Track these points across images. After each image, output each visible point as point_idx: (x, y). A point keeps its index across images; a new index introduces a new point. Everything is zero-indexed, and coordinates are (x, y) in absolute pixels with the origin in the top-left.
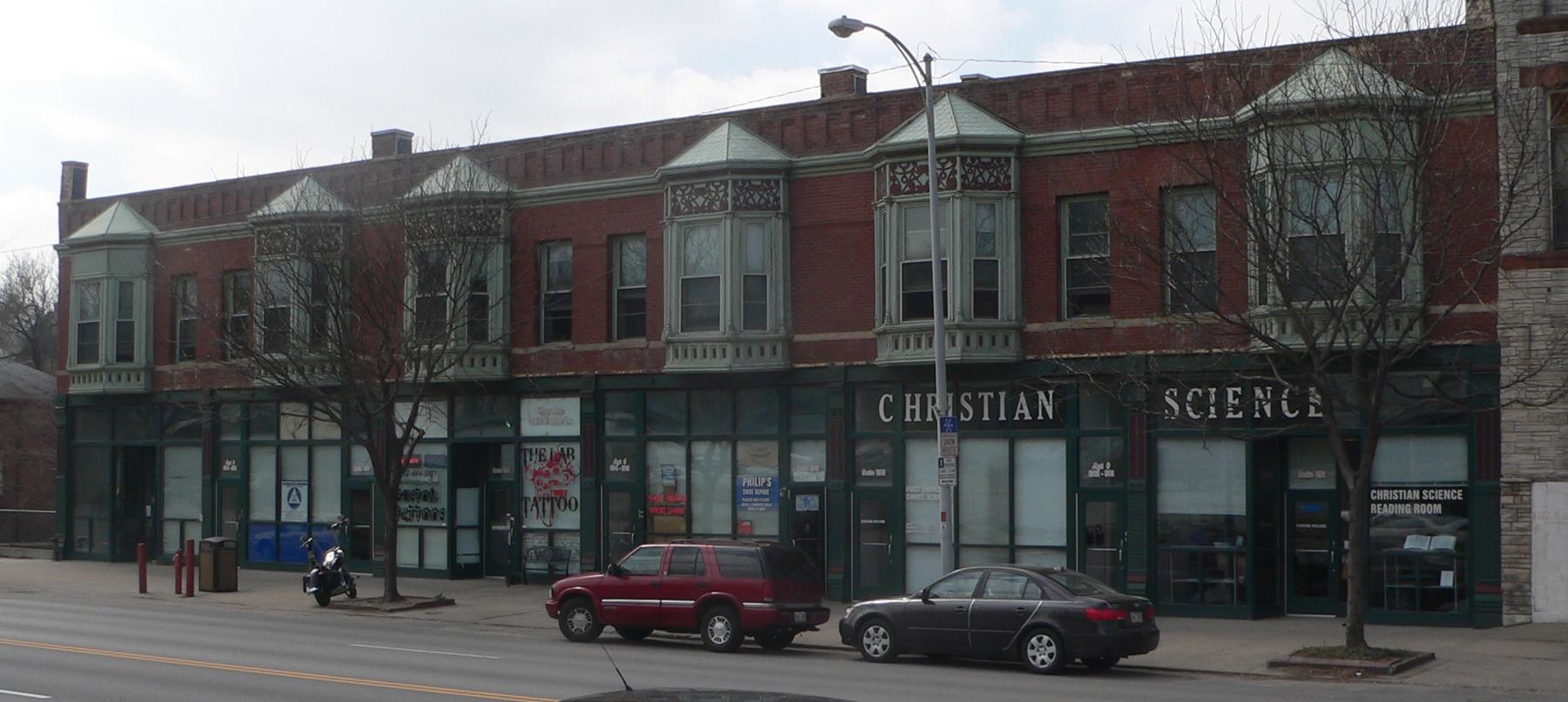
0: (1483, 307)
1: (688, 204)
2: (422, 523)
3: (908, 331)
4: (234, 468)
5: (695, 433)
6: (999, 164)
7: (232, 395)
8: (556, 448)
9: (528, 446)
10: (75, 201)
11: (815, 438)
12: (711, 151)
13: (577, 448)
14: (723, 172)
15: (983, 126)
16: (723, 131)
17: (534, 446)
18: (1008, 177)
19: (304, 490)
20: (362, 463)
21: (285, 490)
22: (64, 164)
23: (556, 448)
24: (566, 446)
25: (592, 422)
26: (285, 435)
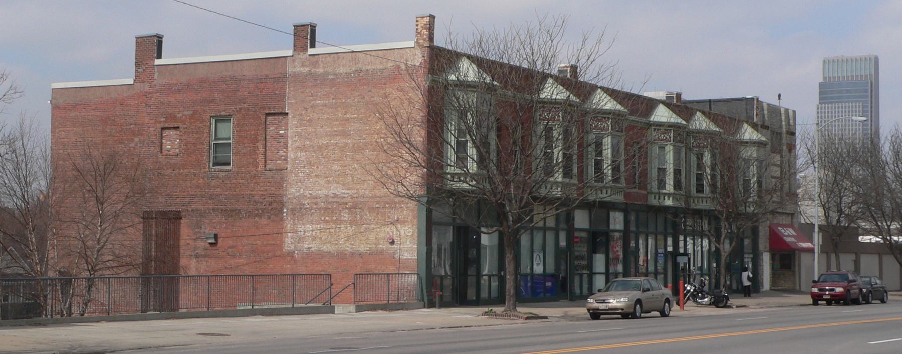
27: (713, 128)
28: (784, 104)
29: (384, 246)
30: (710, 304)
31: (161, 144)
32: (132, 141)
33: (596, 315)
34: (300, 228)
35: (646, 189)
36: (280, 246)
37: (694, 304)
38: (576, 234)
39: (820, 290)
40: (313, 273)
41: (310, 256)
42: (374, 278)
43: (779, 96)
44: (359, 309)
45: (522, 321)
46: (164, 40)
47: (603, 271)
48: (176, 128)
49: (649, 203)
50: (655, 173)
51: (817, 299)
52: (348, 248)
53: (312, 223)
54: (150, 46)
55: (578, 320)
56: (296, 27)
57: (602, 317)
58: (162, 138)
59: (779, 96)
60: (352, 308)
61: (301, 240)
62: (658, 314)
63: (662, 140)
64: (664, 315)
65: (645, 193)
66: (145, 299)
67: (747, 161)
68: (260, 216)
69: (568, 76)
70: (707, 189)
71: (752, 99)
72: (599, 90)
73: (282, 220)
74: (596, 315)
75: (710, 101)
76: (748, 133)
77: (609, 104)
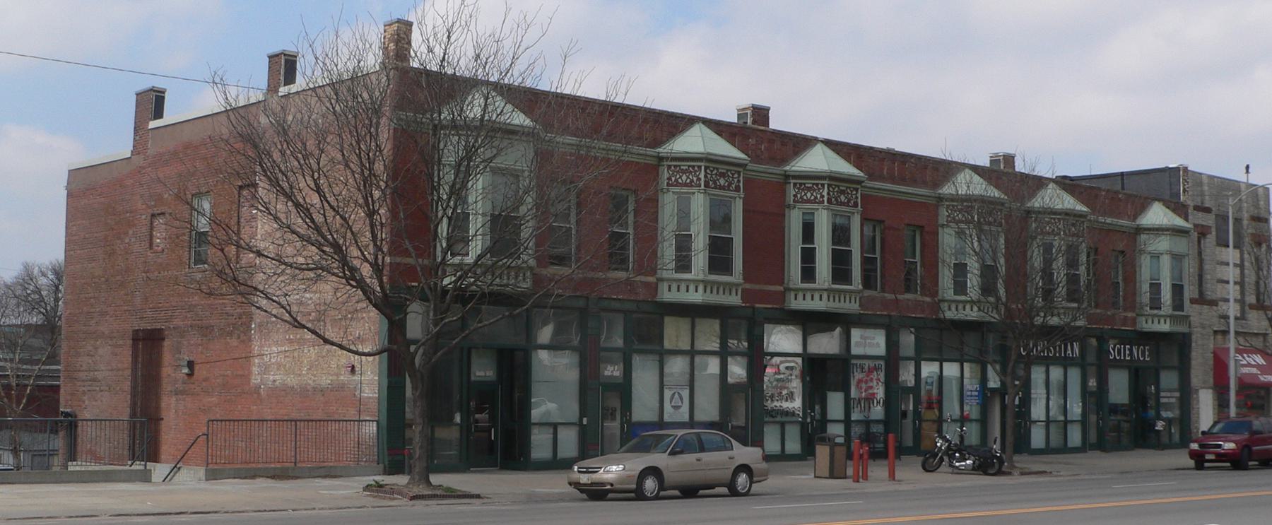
0: (398, 260)
1: (715, 183)
2: (785, 419)
3: (709, 282)
4: (617, 374)
5: (924, 356)
6: (969, 210)
7: (617, 305)
8: (872, 363)
9: (854, 361)
10: (284, 66)
11: (573, 349)
12: (692, 142)
13: (882, 363)
14: (823, 178)
15: (844, 167)
16: (697, 129)
17: (859, 362)
18: (699, 179)
19: (686, 394)
20: (737, 371)
21: (668, 394)
22: (768, 109)
23: (872, 363)
24: (877, 362)
25: (892, 344)
26: (667, 345)
27: (994, 193)
28: (1256, 178)
29: (345, 377)
30: (974, 469)
31: (151, 237)
32: (126, 234)
33: (597, 493)
34: (266, 350)
35: (782, 283)
36: (246, 377)
37: (950, 470)
38: (854, 361)
39: (1201, 446)
40: (279, 417)
41: (281, 392)
42: (336, 426)
43: (1248, 167)
44: (212, 475)
45: (405, 501)
46: (166, 95)
47: (841, 416)
48: (163, 214)
49: (1138, 328)
50: (1146, 287)
51: (1200, 461)
52: (310, 380)
53: (277, 344)
54: (153, 102)
55: (549, 501)
56: (270, 57)
57: (701, 492)
58: (152, 228)
59: (1248, 167)
60: (201, 472)
61: (266, 369)
62: (724, 490)
63: (808, 201)
64: (734, 492)
65: (781, 288)
66: (132, 449)
67: (1156, 257)
68: (230, 334)
69: (749, 121)
70: (700, 260)
71: (1177, 169)
72: (1051, 185)
73: (250, 340)
74: (597, 493)
75: (1122, 174)
76: (1157, 215)
77: (1068, 202)
